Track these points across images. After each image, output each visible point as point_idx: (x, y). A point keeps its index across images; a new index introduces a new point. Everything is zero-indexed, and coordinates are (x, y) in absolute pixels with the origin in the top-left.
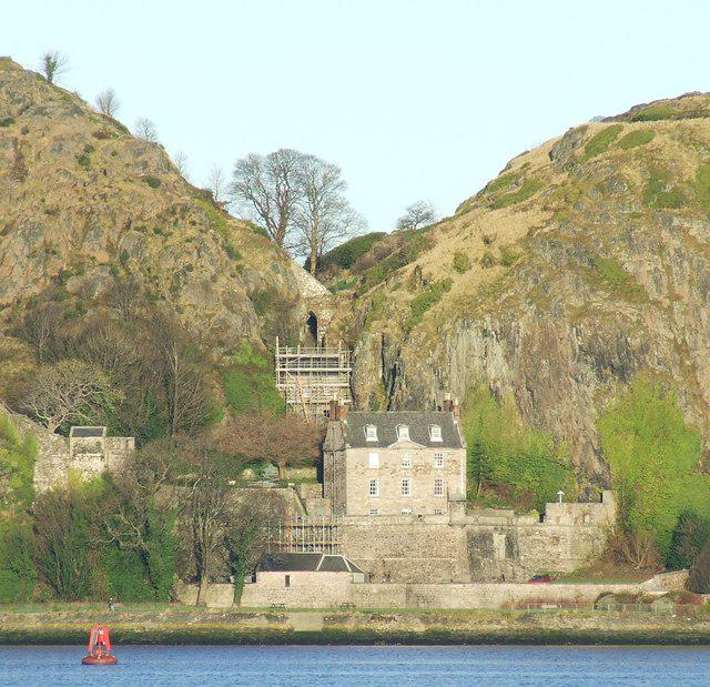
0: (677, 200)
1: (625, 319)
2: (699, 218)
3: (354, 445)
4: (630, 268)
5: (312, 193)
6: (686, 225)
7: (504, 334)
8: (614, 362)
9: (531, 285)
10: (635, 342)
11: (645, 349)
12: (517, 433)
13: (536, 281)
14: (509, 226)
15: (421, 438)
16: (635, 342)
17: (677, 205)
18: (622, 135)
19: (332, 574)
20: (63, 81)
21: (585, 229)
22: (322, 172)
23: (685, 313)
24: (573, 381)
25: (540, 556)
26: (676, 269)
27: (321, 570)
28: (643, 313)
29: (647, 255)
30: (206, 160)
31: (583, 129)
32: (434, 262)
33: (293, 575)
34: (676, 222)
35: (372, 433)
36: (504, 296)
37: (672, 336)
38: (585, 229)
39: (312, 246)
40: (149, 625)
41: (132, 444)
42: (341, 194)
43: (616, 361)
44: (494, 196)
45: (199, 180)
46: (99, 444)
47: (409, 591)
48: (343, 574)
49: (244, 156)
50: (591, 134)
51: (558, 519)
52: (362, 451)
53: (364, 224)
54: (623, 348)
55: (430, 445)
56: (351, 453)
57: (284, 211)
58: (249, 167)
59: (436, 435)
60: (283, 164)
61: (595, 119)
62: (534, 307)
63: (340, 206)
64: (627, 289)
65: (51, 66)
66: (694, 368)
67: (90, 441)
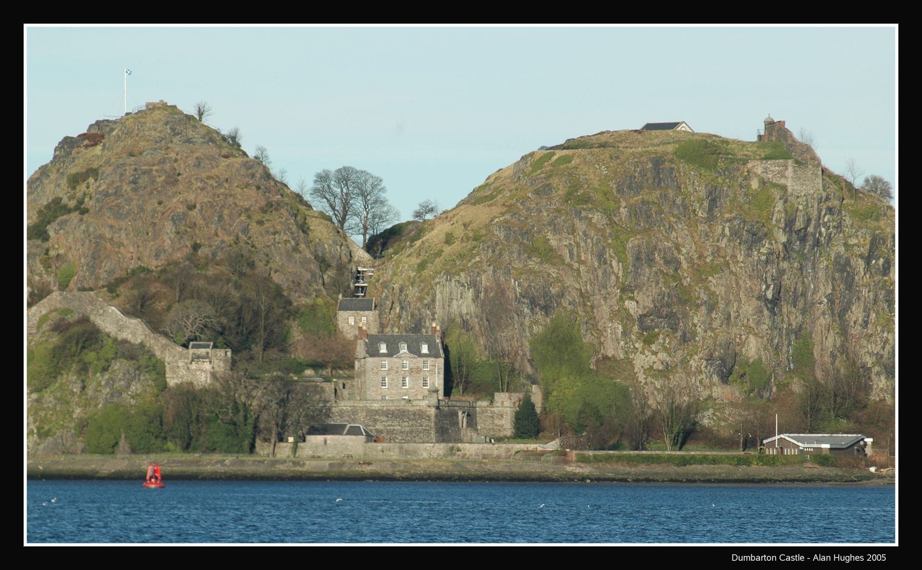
0: (586, 199)
1: (549, 274)
2: (598, 211)
3: (372, 356)
4: (553, 243)
5: (364, 194)
6: (590, 216)
7: (474, 284)
8: (543, 302)
9: (490, 254)
10: (554, 290)
11: (561, 295)
12: (479, 352)
13: (493, 251)
14: (481, 214)
15: (415, 351)
16: (554, 290)
17: (586, 202)
18: (555, 157)
19: (353, 437)
20: (210, 121)
21: (526, 218)
22: (371, 181)
23: (588, 272)
24: (515, 316)
25: (491, 426)
26: (582, 244)
27: (347, 434)
28: (561, 272)
29: (565, 235)
30: (297, 172)
31: (532, 154)
32: (434, 236)
33: (329, 437)
34: (583, 214)
35: (383, 349)
36: (473, 261)
37: (577, 286)
38: (526, 218)
39: (294, 239)
40: (219, 468)
41: (229, 354)
42: (383, 195)
43: (542, 302)
44: (476, 198)
45: (294, 187)
46: (208, 353)
47: (401, 448)
48: (360, 437)
49: (320, 171)
50: (537, 157)
51: (503, 403)
52: (376, 359)
53: (397, 214)
54: (546, 294)
55: (421, 356)
56: (370, 360)
57: (346, 205)
58: (323, 178)
59: (425, 349)
60: (345, 176)
61: (542, 148)
62: (492, 268)
63: (382, 202)
64: (549, 255)
65: (201, 114)
66: (592, 307)
67: (202, 351)
